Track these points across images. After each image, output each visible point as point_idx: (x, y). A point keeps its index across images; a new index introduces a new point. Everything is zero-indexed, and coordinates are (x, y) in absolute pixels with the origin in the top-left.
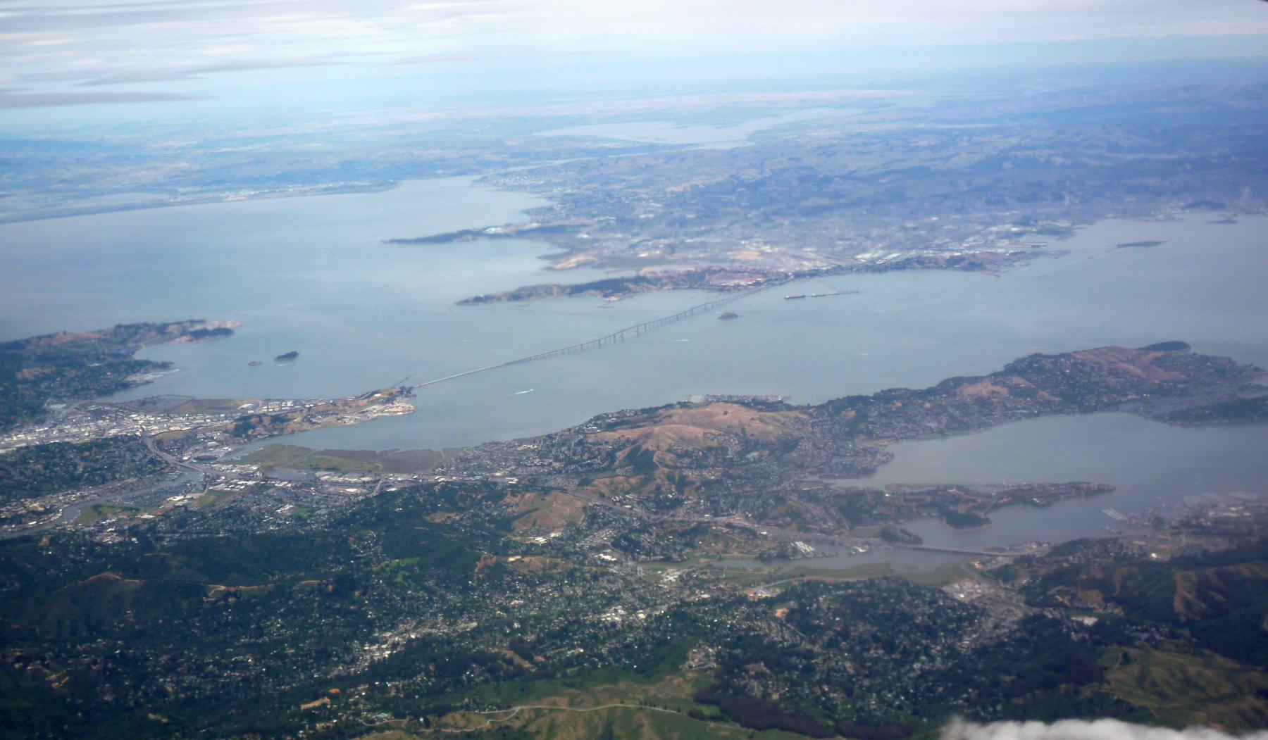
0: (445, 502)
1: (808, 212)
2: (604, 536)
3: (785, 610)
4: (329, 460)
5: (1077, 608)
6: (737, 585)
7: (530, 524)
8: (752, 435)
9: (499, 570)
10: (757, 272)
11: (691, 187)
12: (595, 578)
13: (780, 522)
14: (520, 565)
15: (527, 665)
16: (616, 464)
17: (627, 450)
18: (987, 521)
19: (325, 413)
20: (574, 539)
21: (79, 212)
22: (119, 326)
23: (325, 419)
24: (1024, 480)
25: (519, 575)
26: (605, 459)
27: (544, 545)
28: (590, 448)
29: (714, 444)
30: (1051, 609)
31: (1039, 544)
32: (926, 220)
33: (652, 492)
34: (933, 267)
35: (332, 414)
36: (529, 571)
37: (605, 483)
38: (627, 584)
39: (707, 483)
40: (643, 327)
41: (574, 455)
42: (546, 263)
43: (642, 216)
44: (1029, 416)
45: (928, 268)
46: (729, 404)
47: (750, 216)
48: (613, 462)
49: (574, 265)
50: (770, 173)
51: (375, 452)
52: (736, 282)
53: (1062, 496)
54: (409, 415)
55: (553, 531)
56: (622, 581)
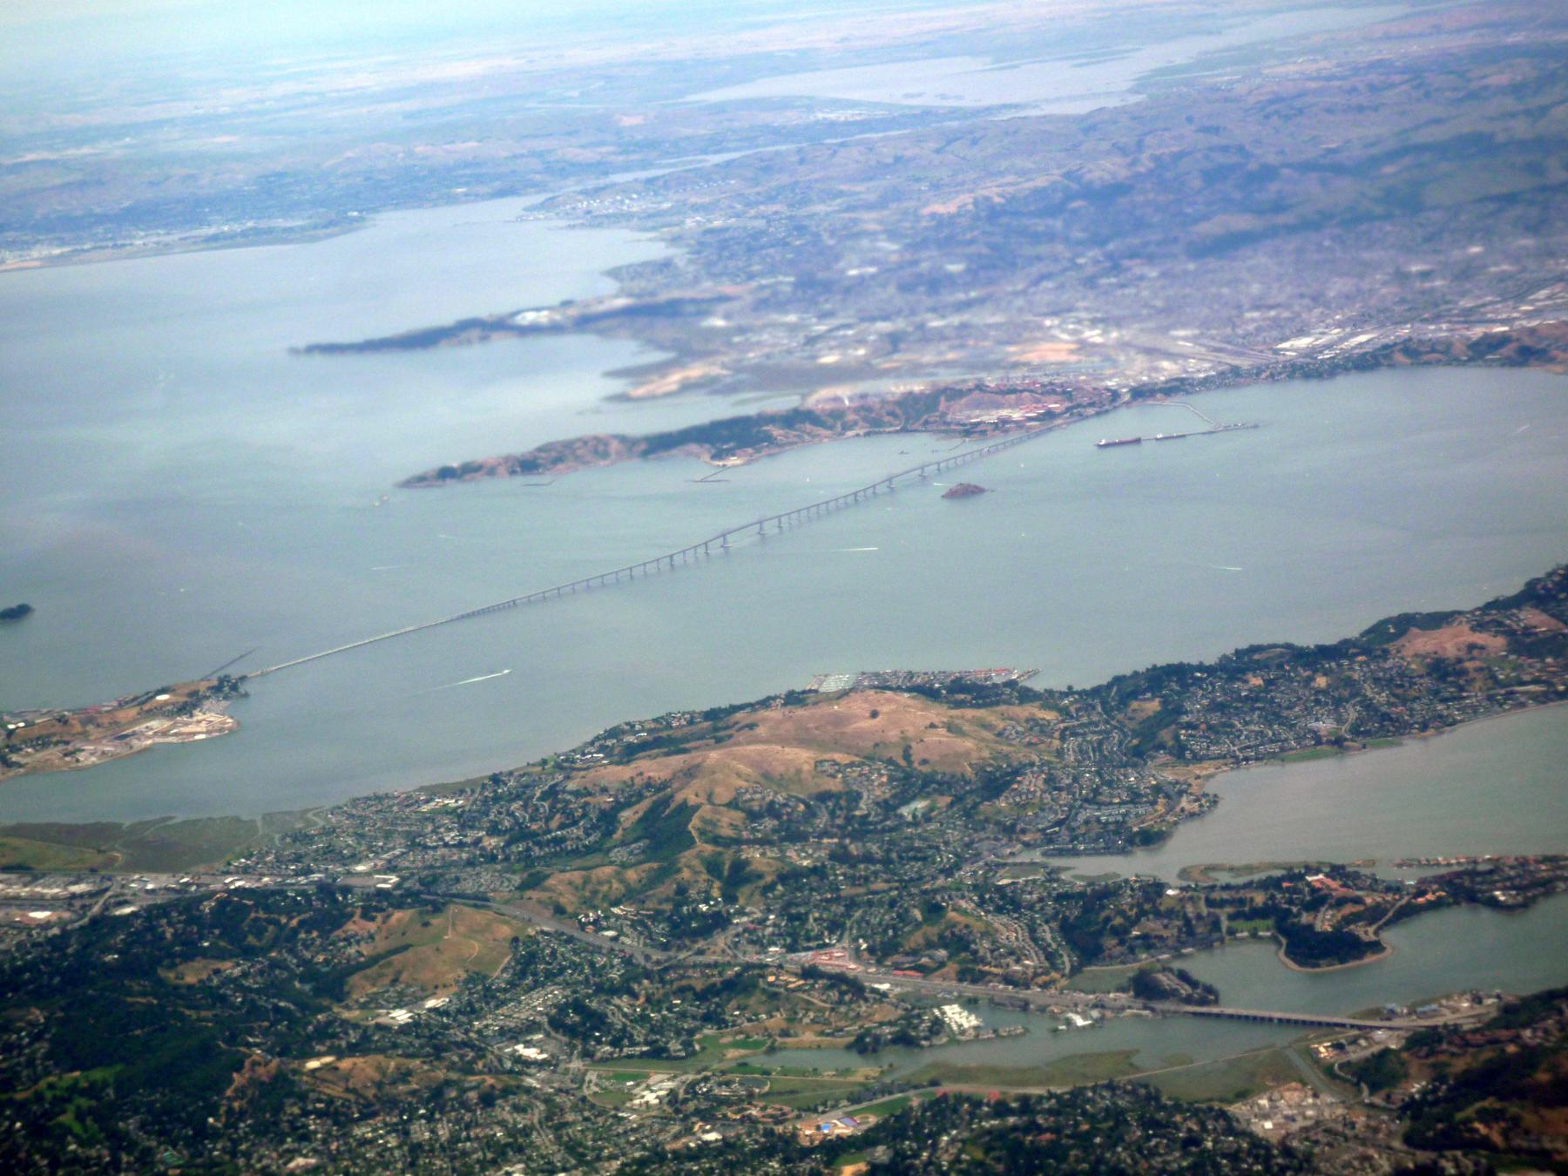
0: (220, 937)
1: (1201, 250)
2: (539, 1002)
4: (15, 849)
5: (1518, 1151)
6: (786, 1109)
7: (387, 981)
8: (925, 762)
9: (281, 1087)
10: (1050, 390)
11: (976, 203)
12: (488, 1100)
13: (924, 960)
14: (329, 1077)
16: (615, 836)
17: (644, 805)
18: (1376, 947)
19: (42, 742)
20: (473, 1011)
23: (39, 755)
24: (1450, 856)
25: (320, 1101)
26: (594, 827)
27: (404, 1029)
28: (568, 802)
29: (834, 785)
30: (1459, 1153)
31: (1477, 1000)
32: (1456, 254)
34: (1438, 362)
35: (57, 743)
36: (347, 1090)
37: (570, 883)
38: (553, 1109)
39: (790, 877)
40: (775, 522)
41: (532, 819)
42: (618, 386)
43: (853, 272)
44: (1542, 699)
45: (1428, 363)
46: (889, 693)
47: (1081, 261)
48: (609, 833)
49: (674, 387)
50: (1151, 165)
51: (120, 826)
52: (1004, 413)
54: (220, 739)
55: (433, 995)
56: (542, 1107)
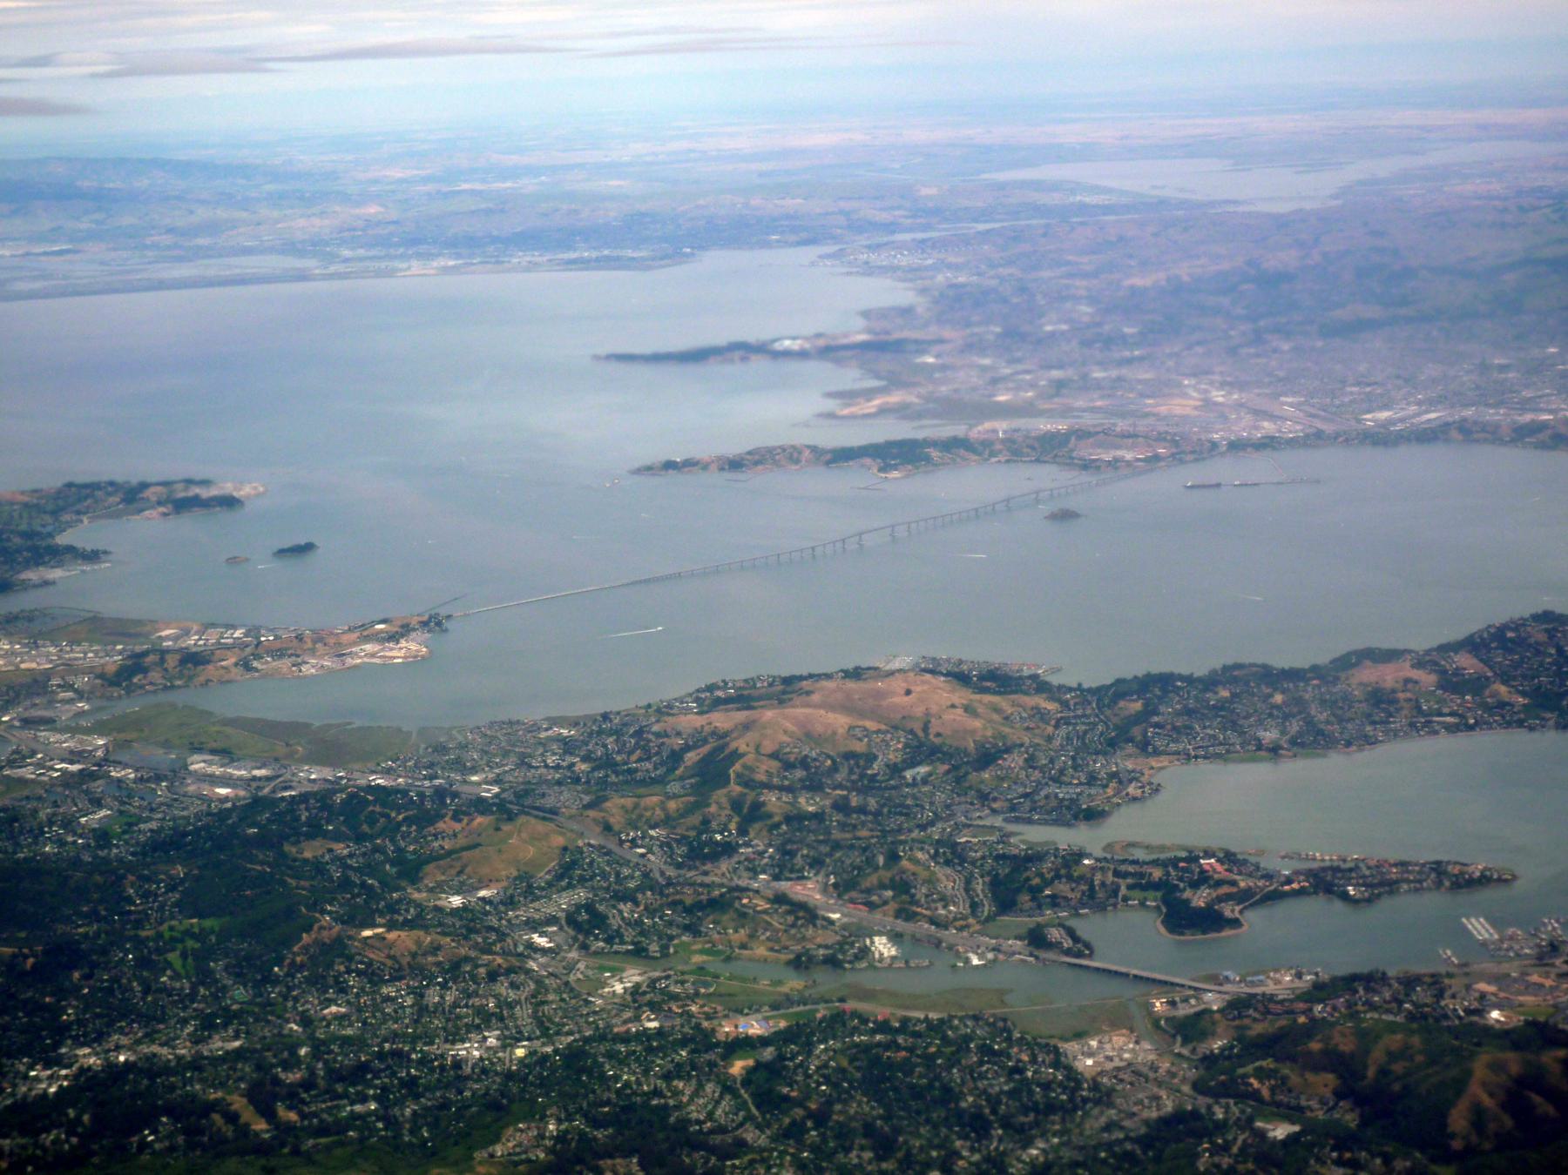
3: (751, 1062)
5: (1279, 1105)
7: (454, 872)
8: (938, 735)
15: (260, 1125)
18: (1235, 923)
21: (161, 285)
22: (70, 485)
24: (1323, 854)
25: (361, 963)
33: (694, 828)
34: (1485, 440)
36: (389, 957)
45: (1477, 441)
48: (672, 769)
49: (873, 410)
53: (1405, 887)
